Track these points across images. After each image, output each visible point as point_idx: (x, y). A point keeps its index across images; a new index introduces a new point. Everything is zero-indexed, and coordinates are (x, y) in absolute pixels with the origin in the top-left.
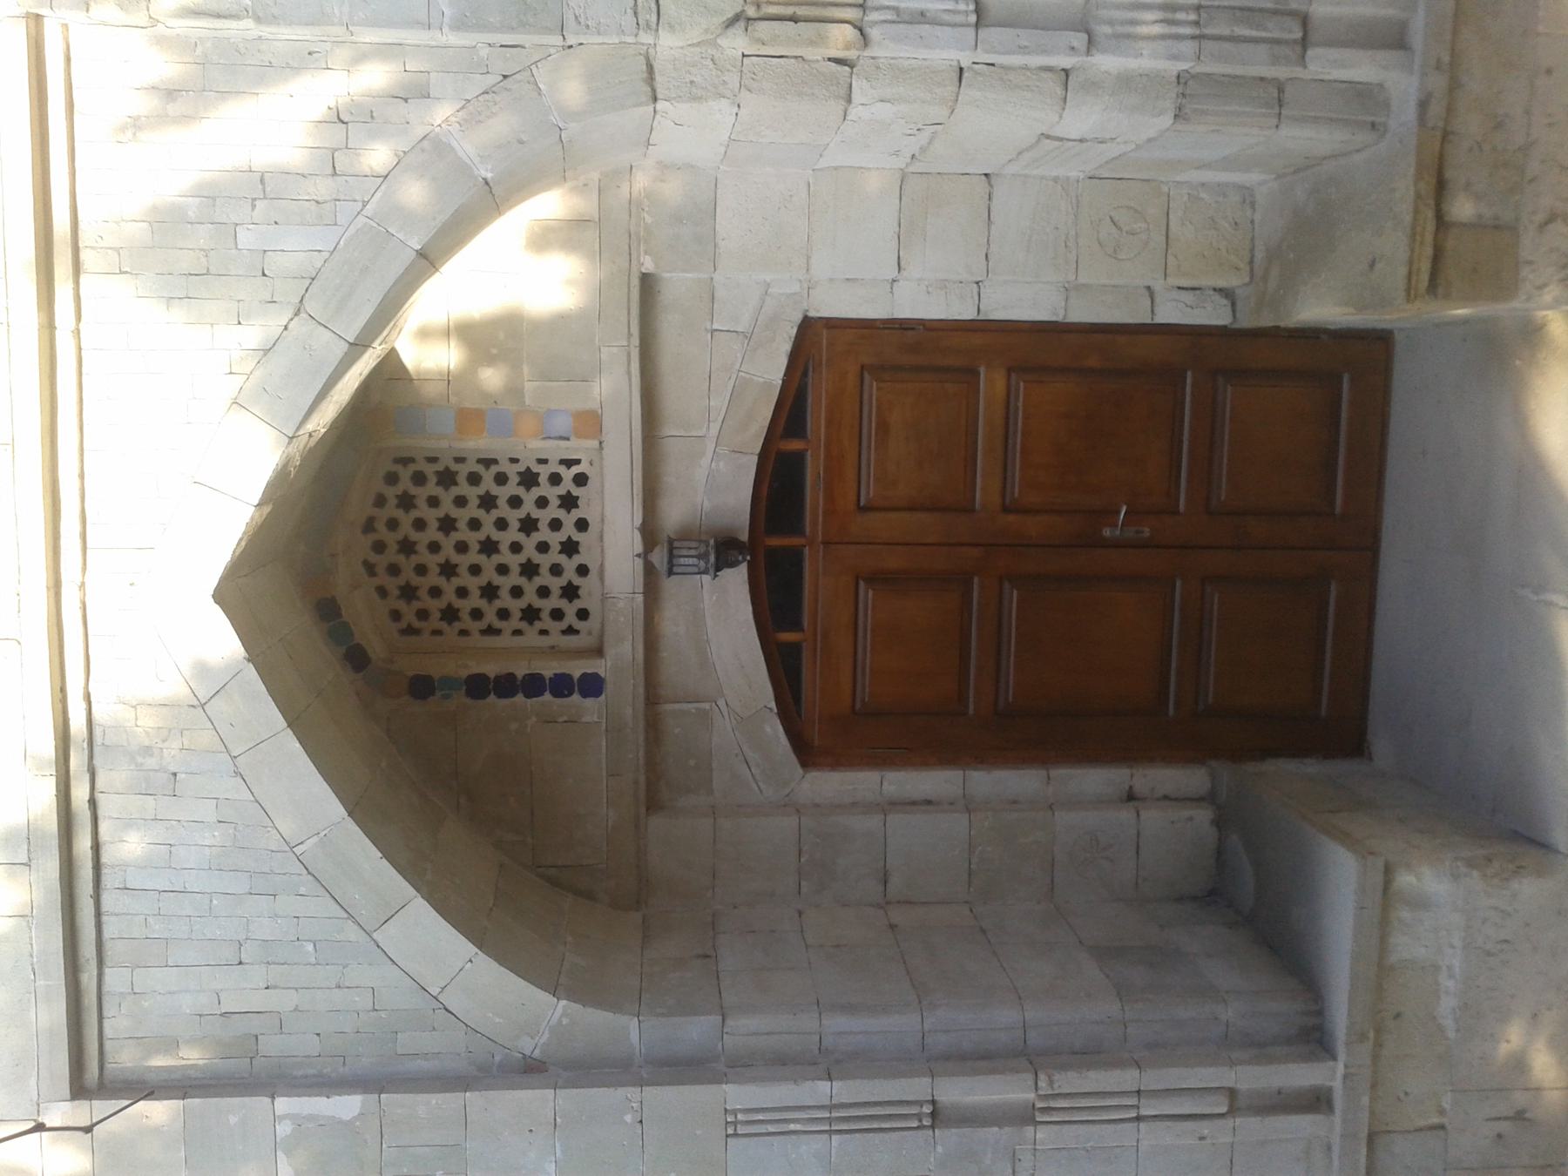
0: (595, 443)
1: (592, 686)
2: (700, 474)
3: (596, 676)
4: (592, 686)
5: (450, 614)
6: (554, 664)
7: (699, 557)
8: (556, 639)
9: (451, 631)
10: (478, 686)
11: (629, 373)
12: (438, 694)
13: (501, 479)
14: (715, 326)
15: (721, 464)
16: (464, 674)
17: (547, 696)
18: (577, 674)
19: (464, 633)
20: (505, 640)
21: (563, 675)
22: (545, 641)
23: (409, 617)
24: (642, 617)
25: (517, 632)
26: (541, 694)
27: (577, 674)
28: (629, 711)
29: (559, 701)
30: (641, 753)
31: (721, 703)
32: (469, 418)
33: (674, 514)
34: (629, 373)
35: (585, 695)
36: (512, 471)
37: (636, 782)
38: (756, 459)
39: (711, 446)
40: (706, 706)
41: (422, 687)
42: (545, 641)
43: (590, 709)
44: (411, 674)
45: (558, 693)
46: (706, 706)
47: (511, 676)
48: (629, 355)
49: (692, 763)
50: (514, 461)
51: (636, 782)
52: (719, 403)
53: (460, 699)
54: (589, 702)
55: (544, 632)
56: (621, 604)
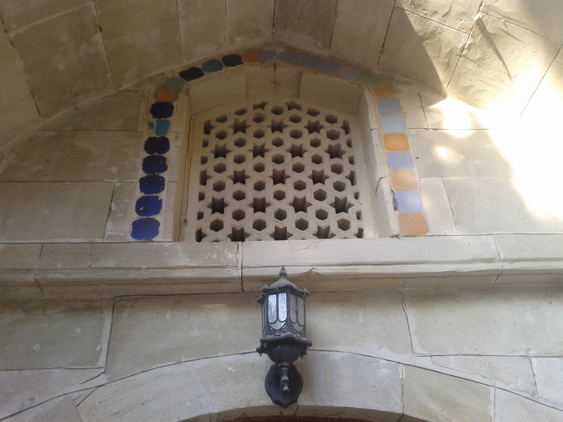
0: (396, 232)
1: (144, 229)
2: (372, 348)
3: (155, 232)
4: (144, 229)
5: (221, 153)
6: (172, 201)
7: (288, 321)
8: (193, 225)
9: (208, 152)
10: (157, 147)
11: (473, 261)
12: (155, 120)
13: (339, 187)
14: (534, 360)
15: (385, 371)
16: (170, 137)
17: (139, 194)
18: (159, 218)
19: (204, 161)
20: (195, 187)
21: (161, 208)
22: (192, 216)
23: (219, 128)
24: (216, 276)
25: (202, 197)
26: (142, 189)
27: (159, 218)
28: (111, 264)
29: (133, 204)
30: (60, 276)
31: (103, 379)
32: (399, 142)
33: (328, 325)
34: (473, 261)
35: (135, 224)
36: (348, 194)
37: (28, 271)
38: (398, 410)
39: (404, 358)
40: (101, 362)
41: (162, 110)
42: (192, 216)
43: (121, 228)
44: (175, 104)
45: (140, 203)
46: (101, 362)
47: (164, 168)
48: (491, 260)
49: (37, 347)
50: (356, 196)
51: (28, 271)
52: (454, 366)
53: (147, 134)
54: (128, 228)
55: (200, 216)
56: (230, 256)
